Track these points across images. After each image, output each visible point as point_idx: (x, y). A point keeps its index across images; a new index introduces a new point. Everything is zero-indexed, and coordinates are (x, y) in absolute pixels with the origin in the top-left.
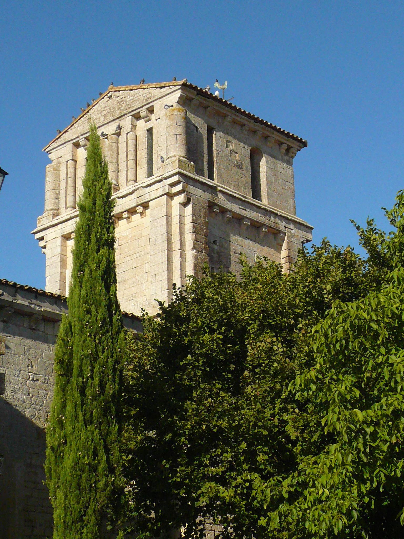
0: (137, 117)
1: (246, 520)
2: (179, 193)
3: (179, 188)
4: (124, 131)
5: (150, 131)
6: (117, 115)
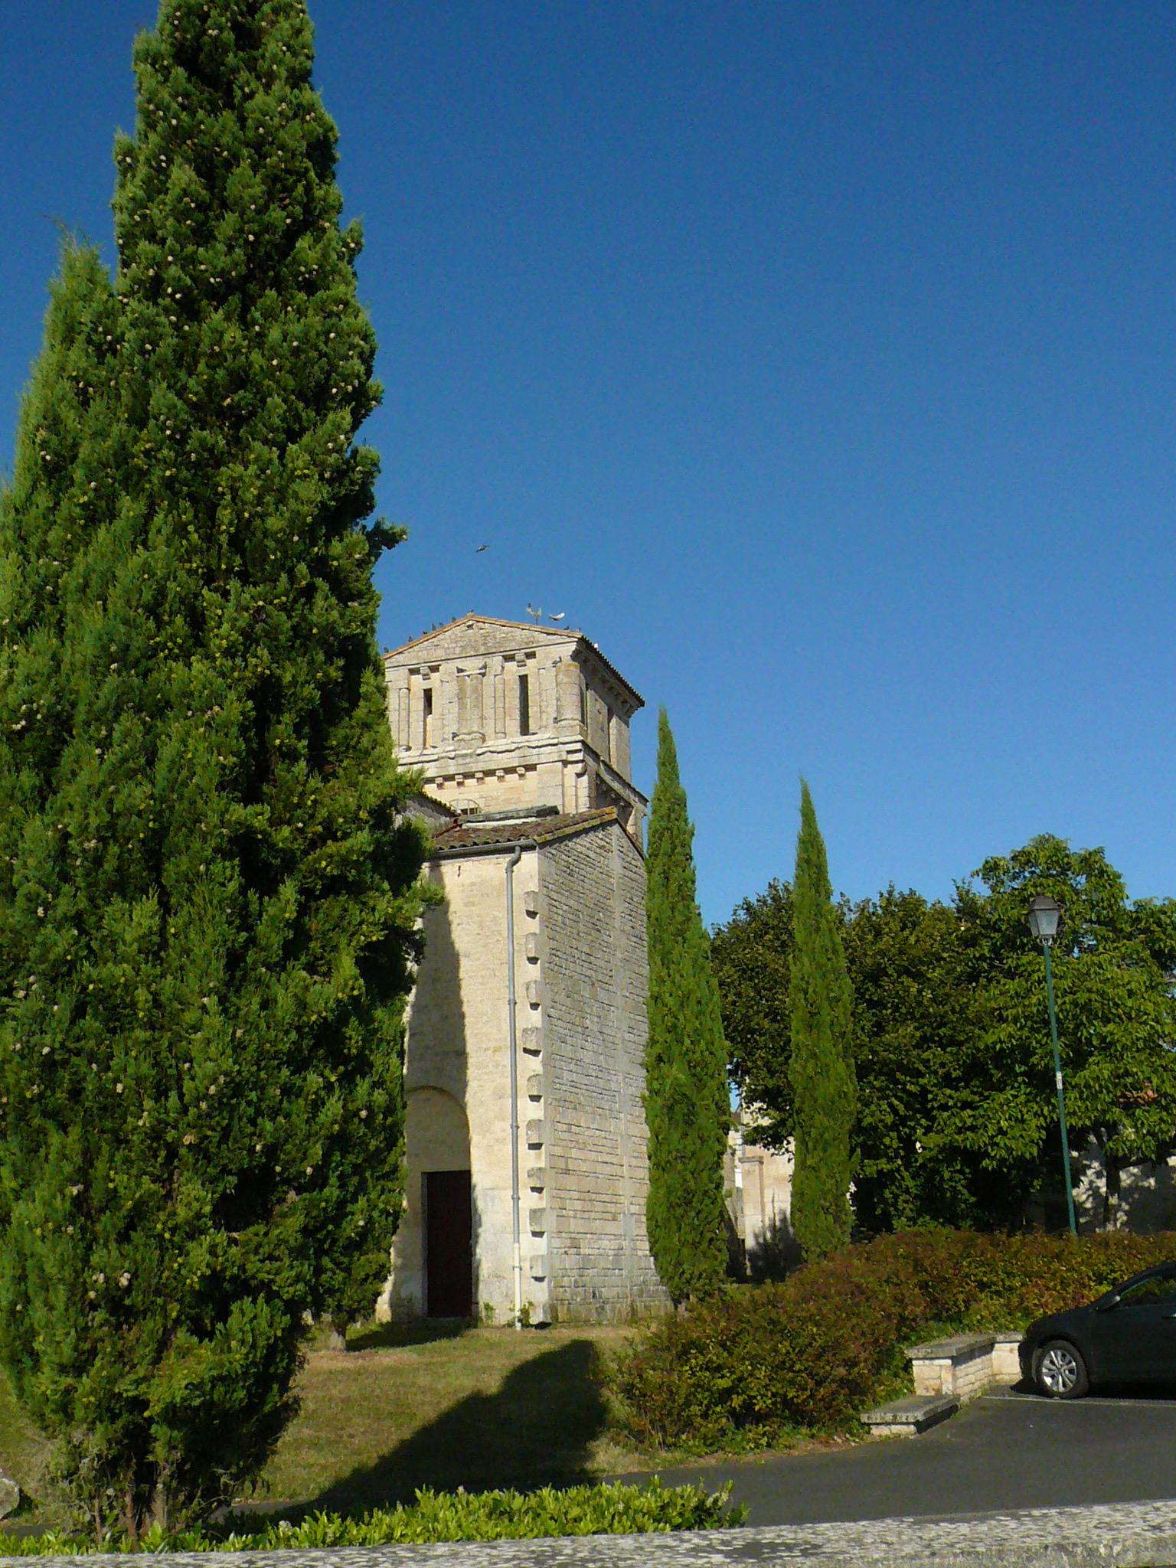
0: (509, 658)
1: (190, 1146)
2: (577, 762)
3: (579, 756)
4: (491, 672)
5: (523, 679)
6: (482, 650)
